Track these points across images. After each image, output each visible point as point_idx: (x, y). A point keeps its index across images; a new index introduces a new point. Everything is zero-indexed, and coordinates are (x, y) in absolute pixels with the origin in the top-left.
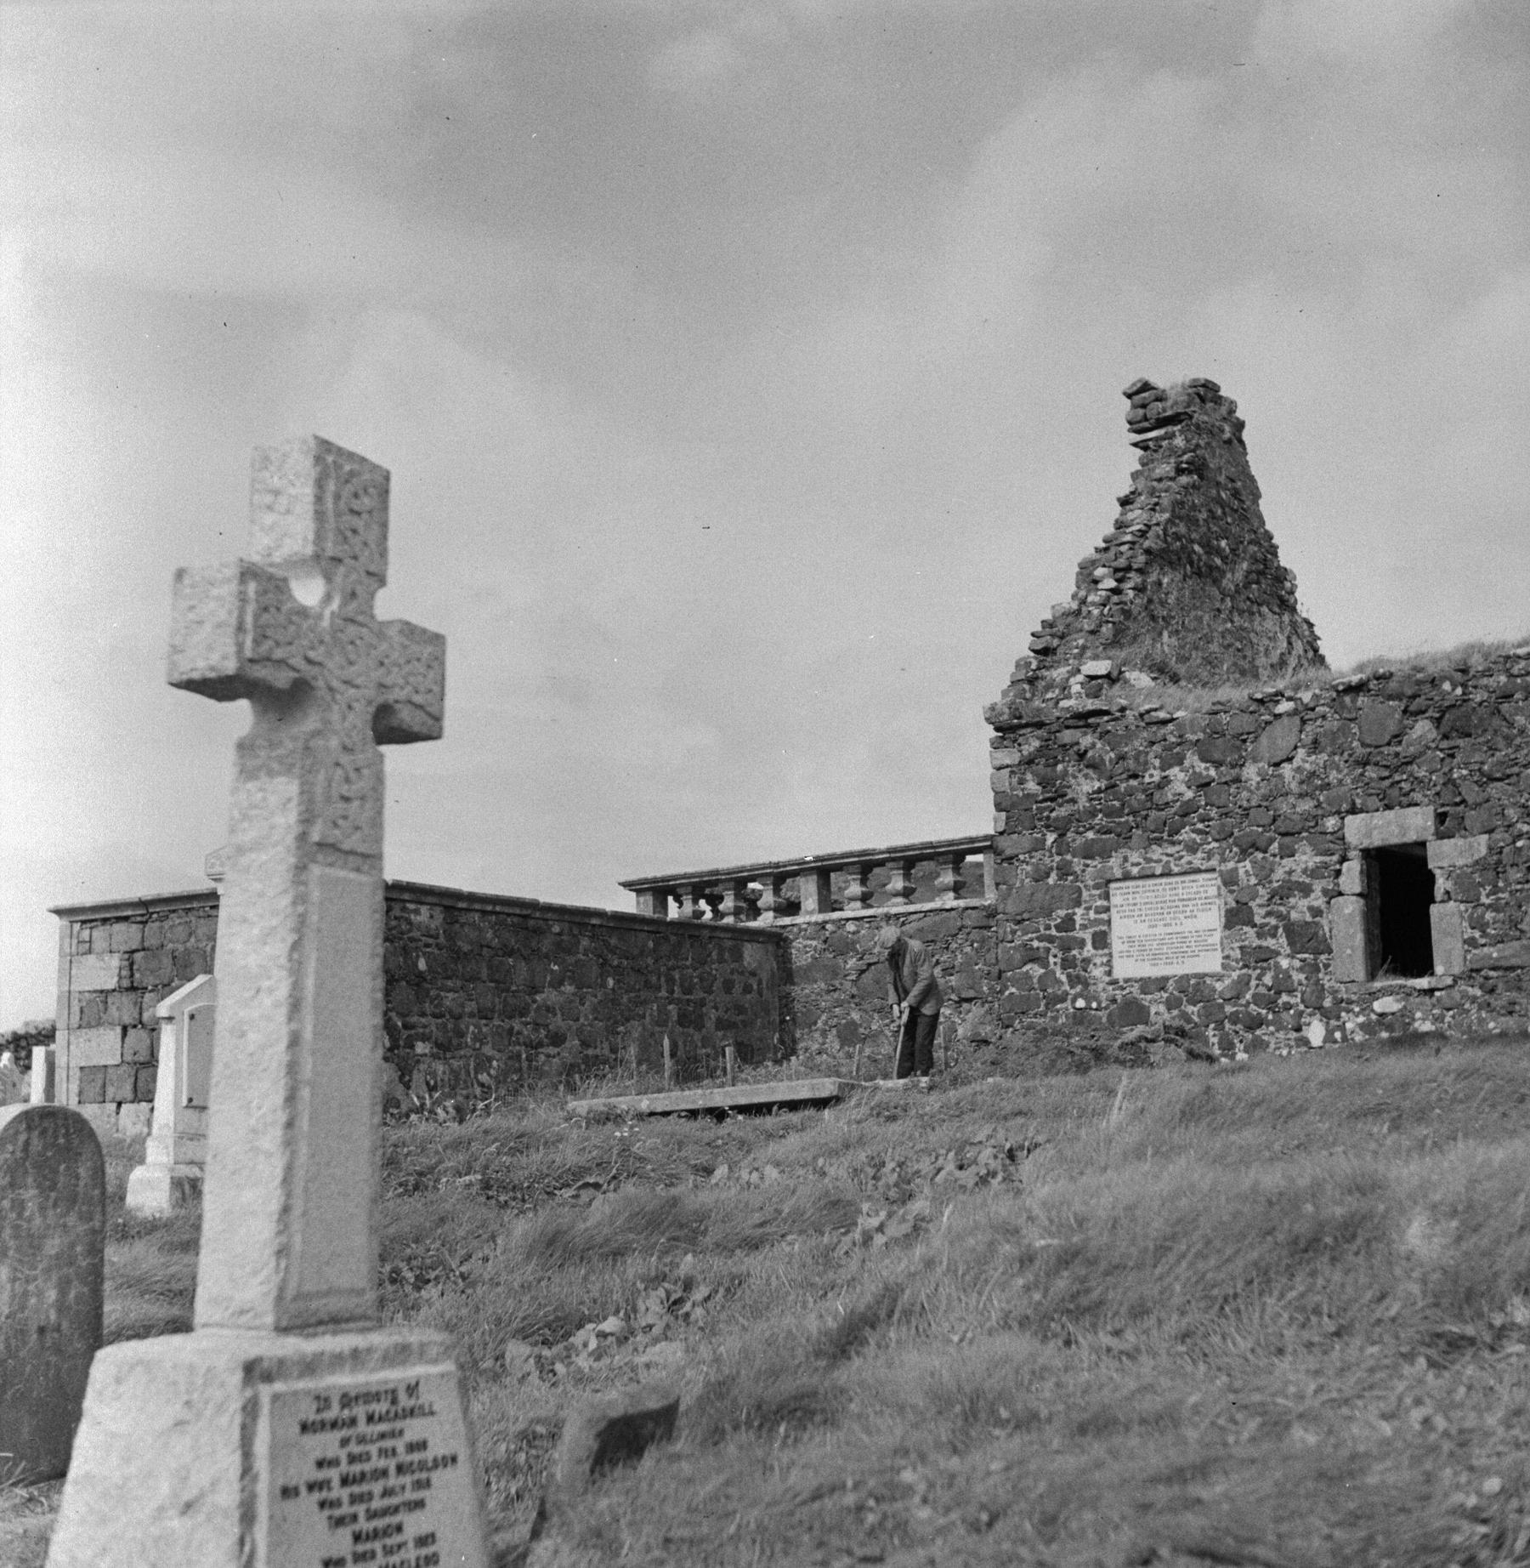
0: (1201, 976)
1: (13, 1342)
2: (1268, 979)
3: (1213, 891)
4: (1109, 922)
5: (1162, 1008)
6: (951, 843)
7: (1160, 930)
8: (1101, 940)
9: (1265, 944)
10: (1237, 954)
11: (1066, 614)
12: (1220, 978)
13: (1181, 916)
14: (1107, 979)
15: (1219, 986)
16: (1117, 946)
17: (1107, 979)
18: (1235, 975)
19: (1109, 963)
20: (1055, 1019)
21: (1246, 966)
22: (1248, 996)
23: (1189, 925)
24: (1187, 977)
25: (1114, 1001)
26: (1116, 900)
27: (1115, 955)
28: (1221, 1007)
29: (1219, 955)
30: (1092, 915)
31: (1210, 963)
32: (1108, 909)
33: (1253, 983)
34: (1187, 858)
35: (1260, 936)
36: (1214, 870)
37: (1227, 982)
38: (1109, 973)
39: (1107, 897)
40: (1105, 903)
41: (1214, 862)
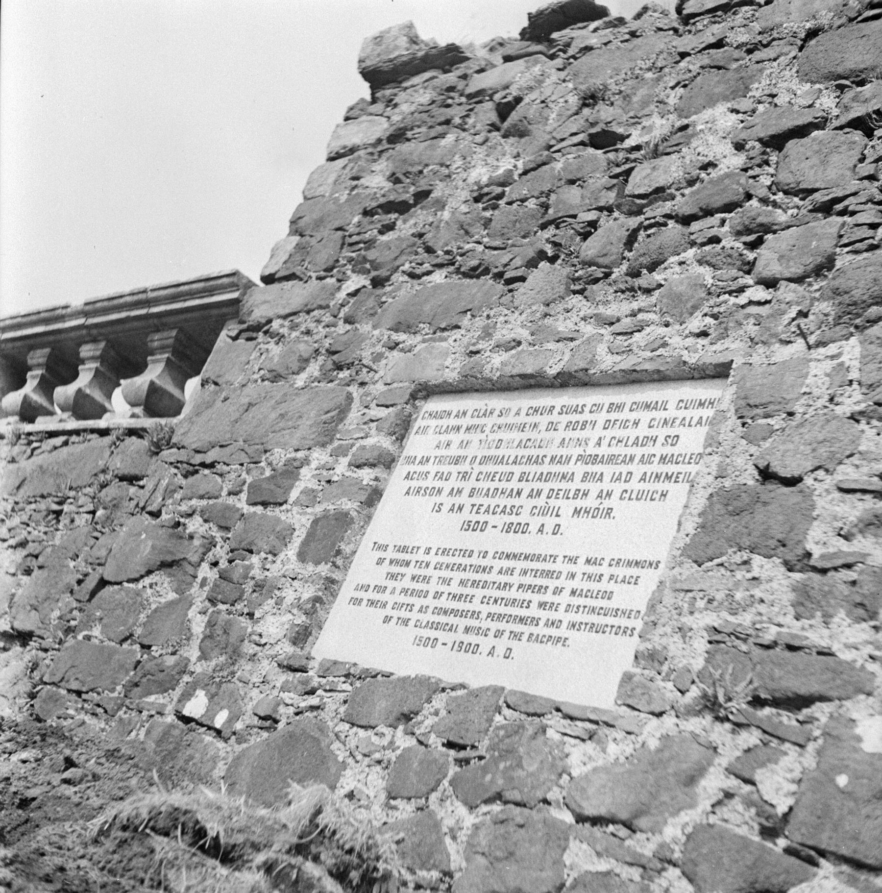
0: (535, 711)
1: (669, 598)
2: (777, 786)
3: (692, 440)
4: (374, 496)
5: (375, 783)
6: (177, 291)
7: (493, 540)
8: (330, 541)
9: (816, 635)
10: (693, 655)
11: (848, 698)
12: (594, 726)
13: (567, 507)
14: (286, 649)
15: (580, 758)
16: (364, 568)
17: (286, 649)
18: (653, 732)
19: (315, 608)
20: (126, 728)
21: (711, 706)
22: (673, 831)
23: (579, 537)
24: (497, 699)
25: (269, 720)
26: (417, 444)
27: (346, 592)
28: (558, 839)
29: (621, 654)
30: (342, 467)
31: (585, 672)
32: (387, 462)
33: (714, 782)
34: (656, 331)
35: (805, 603)
36: (721, 371)
37: (617, 749)
38: (301, 636)
39: (401, 430)
40: (386, 443)
41: (732, 348)
